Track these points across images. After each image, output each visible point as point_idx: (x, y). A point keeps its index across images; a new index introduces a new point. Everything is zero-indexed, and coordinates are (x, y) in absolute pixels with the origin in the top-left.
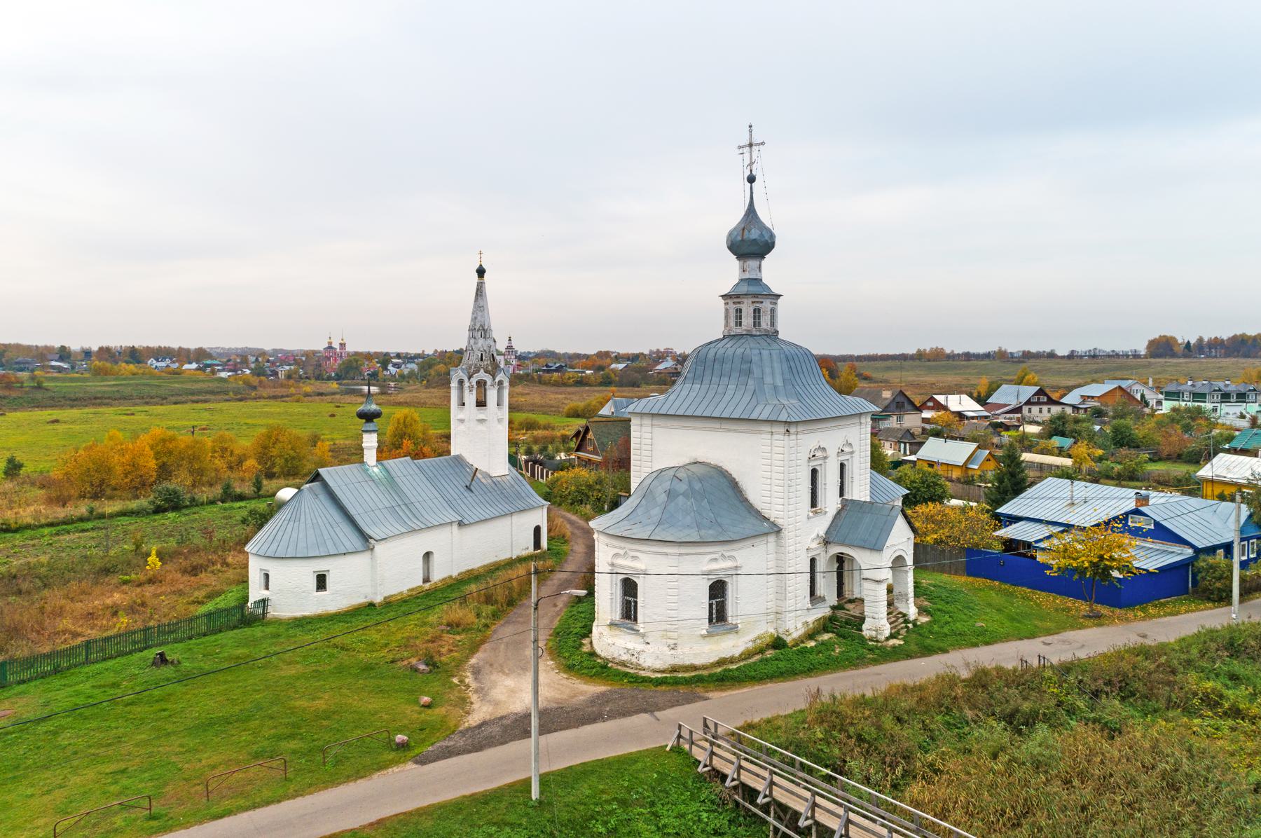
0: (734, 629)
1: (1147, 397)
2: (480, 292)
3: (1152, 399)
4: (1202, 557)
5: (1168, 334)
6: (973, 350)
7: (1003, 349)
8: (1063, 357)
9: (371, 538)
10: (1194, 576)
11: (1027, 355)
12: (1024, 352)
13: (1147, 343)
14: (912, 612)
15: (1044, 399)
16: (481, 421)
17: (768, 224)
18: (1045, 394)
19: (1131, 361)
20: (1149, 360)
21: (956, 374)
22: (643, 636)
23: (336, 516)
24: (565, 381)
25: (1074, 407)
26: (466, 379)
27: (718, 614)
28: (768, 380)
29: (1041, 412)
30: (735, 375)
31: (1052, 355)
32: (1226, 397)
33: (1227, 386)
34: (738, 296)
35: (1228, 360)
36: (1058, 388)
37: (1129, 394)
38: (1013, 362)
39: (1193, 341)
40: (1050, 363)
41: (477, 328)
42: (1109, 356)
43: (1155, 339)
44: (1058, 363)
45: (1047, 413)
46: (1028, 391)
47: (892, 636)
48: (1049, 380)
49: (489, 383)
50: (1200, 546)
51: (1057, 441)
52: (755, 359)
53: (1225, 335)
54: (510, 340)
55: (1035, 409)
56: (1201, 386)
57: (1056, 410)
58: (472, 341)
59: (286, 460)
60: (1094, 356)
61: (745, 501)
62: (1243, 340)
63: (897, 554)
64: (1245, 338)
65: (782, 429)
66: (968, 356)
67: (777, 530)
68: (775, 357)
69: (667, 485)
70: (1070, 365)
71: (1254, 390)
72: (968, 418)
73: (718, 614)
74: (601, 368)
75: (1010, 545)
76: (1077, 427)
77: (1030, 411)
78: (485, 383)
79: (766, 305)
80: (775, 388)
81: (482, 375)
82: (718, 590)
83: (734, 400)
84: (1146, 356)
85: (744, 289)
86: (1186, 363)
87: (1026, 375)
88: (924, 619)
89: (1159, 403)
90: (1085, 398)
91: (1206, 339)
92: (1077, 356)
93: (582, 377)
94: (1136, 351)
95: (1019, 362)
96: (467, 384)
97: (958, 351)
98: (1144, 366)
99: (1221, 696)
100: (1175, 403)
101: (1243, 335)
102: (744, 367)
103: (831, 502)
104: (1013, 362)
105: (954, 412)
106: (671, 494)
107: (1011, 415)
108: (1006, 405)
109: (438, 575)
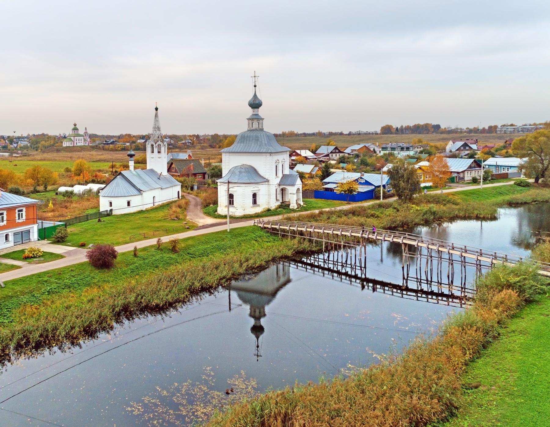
0: (259, 206)
1: (376, 150)
2: (156, 116)
3: (378, 151)
4: (376, 188)
5: (389, 124)
6: (306, 132)
7: (320, 131)
8: (346, 135)
9: (142, 191)
10: (375, 193)
11: (331, 134)
12: (329, 132)
13: (380, 128)
14: (302, 204)
15: (337, 151)
16: (159, 158)
17: (260, 99)
18: (338, 149)
19: (375, 136)
20: (381, 135)
21: (300, 143)
22: (236, 208)
23: (380, 253)
24: (116, 148)
25: (349, 154)
26: (154, 144)
27: (255, 202)
28: (263, 142)
29: (336, 156)
30: (254, 141)
31: (341, 134)
32: (402, 149)
33: (403, 145)
34: (253, 119)
35: (412, 135)
36: (342, 148)
37: (368, 148)
38: (325, 137)
39: (399, 127)
40: (340, 137)
41: (156, 127)
42: (365, 134)
43: (384, 126)
44: (344, 137)
45: (337, 156)
46: (331, 148)
47: (297, 208)
48: (339, 145)
49: (162, 145)
50: (376, 185)
51: (342, 165)
52: (259, 136)
53: (412, 124)
54: (86, 129)
55: (334, 155)
56: (394, 145)
57: (341, 155)
58: (155, 132)
59: (45, 179)
60: (359, 134)
61: (259, 174)
62: (418, 127)
63: (298, 187)
64: (419, 126)
65: (269, 155)
66: (305, 135)
67: (268, 181)
68: (265, 136)
69: (239, 170)
70: (349, 138)
71: (412, 146)
72: (309, 159)
73: (255, 202)
74: (134, 142)
75: (327, 189)
76: (349, 160)
77: (332, 156)
78: (160, 145)
79: (261, 121)
80: (265, 144)
81: (159, 143)
82: (254, 195)
83: (254, 147)
84: (380, 134)
85: (254, 117)
86: (396, 136)
87: (330, 142)
88: (305, 205)
89: (380, 152)
90: (353, 150)
91: (404, 126)
92: (352, 134)
93: (125, 147)
94: (376, 132)
95: (327, 137)
96: (154, 146)
97: (300, 132)
98: (379, 138)
99: (375, 214)
100: (385, 152)
101: (419, 124)
102: (256, 138)
103: (280, 175)
104: (325, 137)
105: (303, 157)
106: (240, 172)
107: (325, 158)
108: (323, 154)
109: (156, 204)
